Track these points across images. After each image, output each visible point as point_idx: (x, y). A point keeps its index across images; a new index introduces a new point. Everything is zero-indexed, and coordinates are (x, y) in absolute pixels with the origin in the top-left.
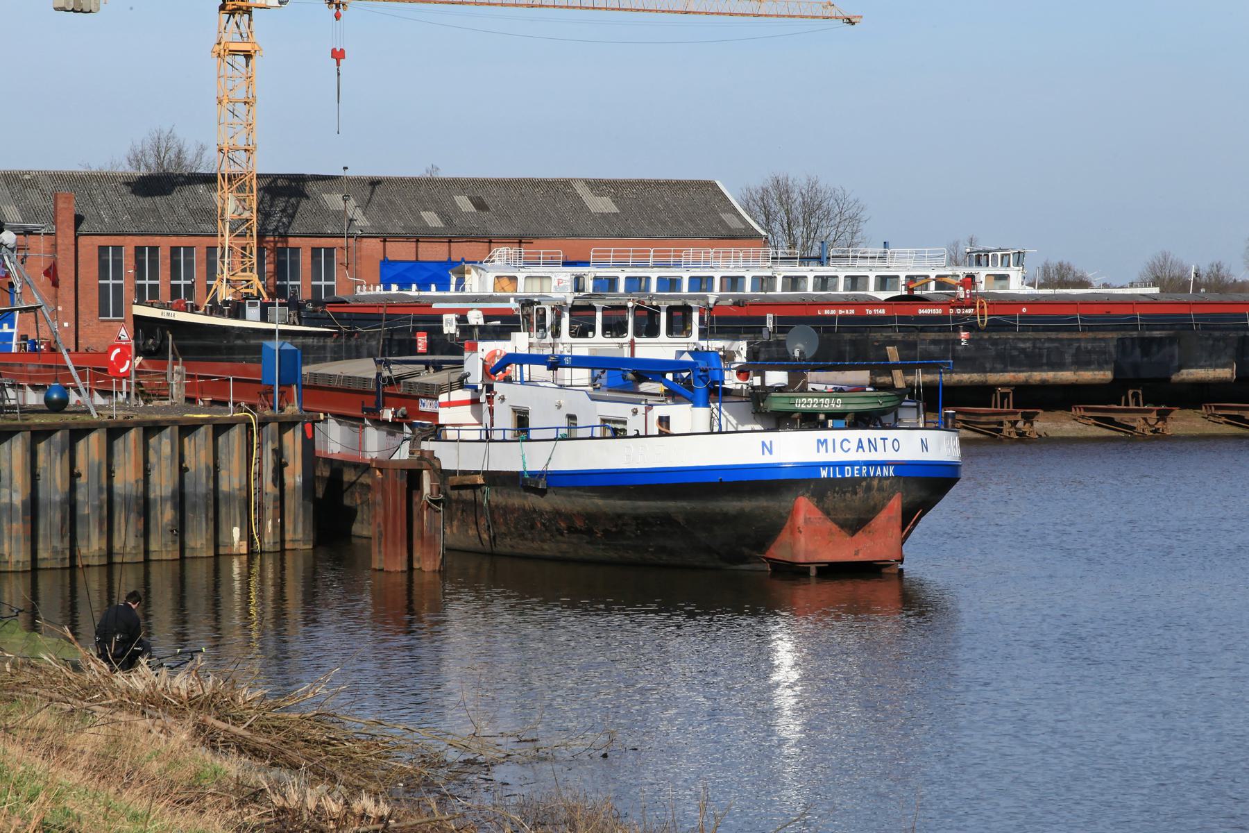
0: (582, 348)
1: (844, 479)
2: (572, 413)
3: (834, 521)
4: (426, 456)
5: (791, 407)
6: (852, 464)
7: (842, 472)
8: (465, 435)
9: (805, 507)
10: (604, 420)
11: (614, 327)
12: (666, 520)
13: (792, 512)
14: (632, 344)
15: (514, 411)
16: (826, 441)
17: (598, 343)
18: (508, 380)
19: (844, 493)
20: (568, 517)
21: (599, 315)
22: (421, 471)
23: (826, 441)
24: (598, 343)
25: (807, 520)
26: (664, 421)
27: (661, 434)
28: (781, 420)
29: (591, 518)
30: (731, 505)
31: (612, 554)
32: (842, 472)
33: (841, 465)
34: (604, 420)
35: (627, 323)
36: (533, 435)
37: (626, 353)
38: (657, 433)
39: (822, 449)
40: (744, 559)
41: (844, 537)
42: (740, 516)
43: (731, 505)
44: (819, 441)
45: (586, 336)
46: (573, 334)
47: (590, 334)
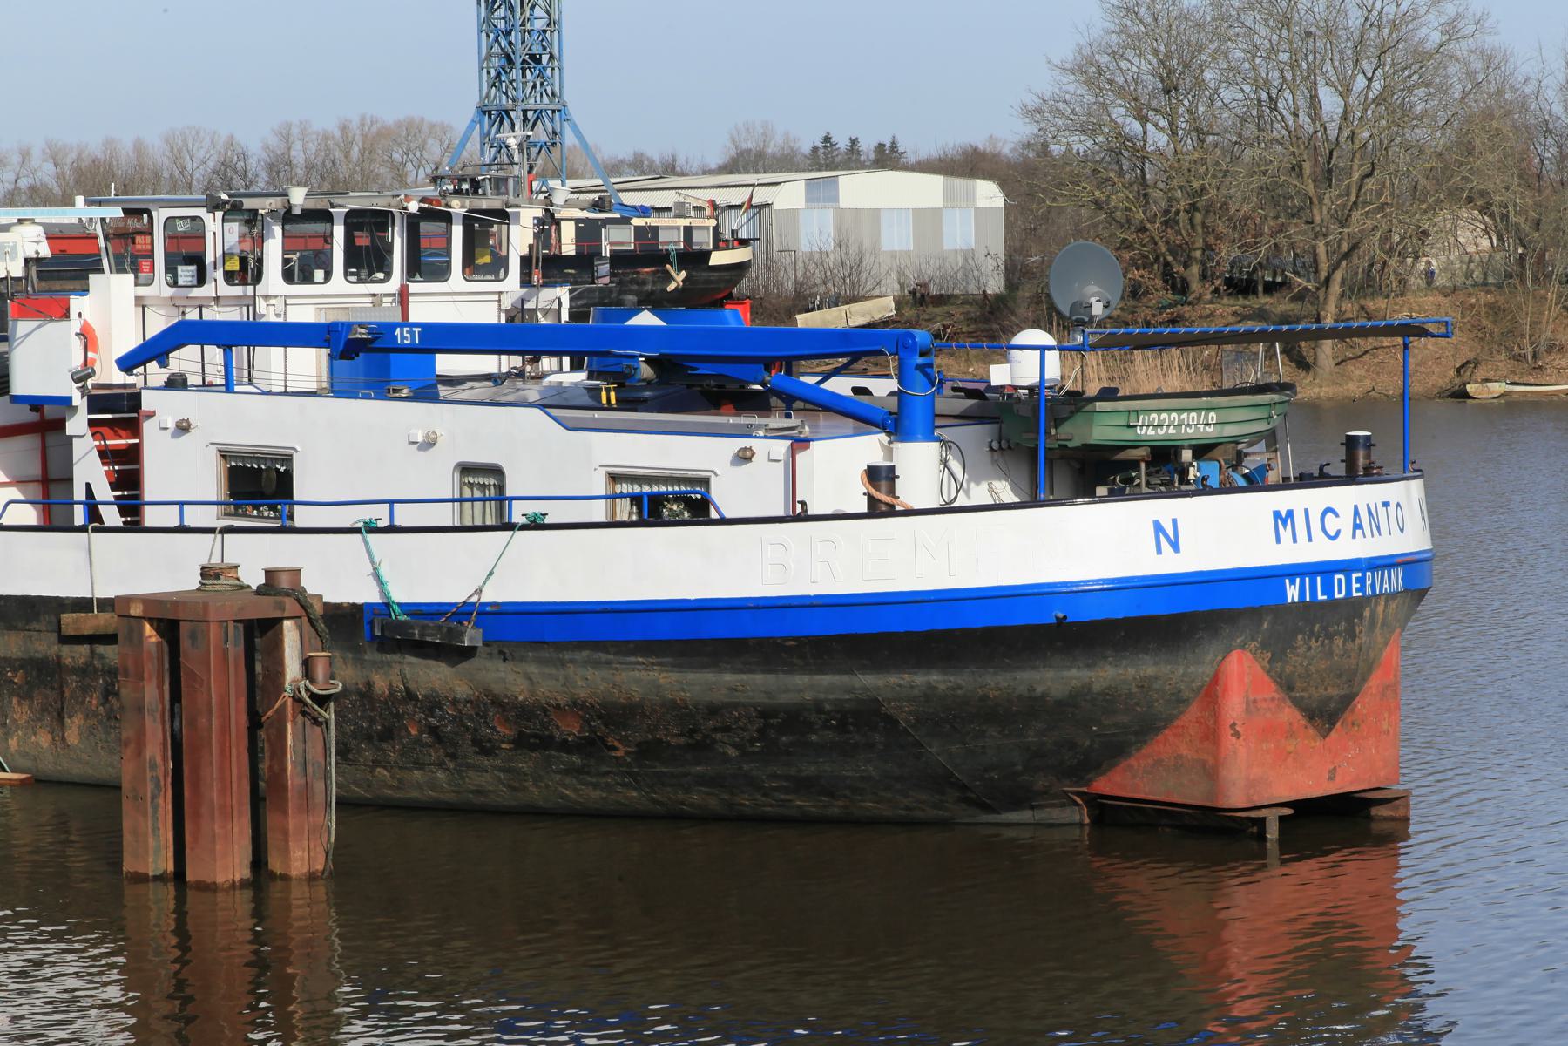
0: (303, 306)
1: (1332, 604)
2: (748, 466)
3: (1296, 702)
4: (284, 582)
5: (1128, 435)
6: (1347, 567)
7: (1328, 588)
8: (194, 517)
9: (1241, 673)
10: (614, 478)
11: (367, 260)
12: (864, 717)
13: (1211, 693)
14: (403, 297)
15: (225, 455)
16: (1290, 513)
17: (339, 295)
18: (176, 383)
19: (1330, 637)
20: (525, 712)
21: (339, 231)
22: (280, 620)
23: (1290, 513)
24: (339, 295)
25: (1251, 706)
26: (880, 476)
27: (876, 510)
28: (1100, 472)
29: (616, 715)
30: (1055, 679)
31: (592, 796)
32: (1328, 588)
33: (1325, 570)
34: (614, 478)
35: (389, 249)
36: (151, 517)
37: (390, 313)
38: (863, 507)
39: (1286, 534)
40: (1021, 798)
41: (1309, 740)
42: (1034, 707)
43: (1055, 679)
44: (1277, 514)
45: (307, 279)
46: (288, 276)
47: (319, 275)
